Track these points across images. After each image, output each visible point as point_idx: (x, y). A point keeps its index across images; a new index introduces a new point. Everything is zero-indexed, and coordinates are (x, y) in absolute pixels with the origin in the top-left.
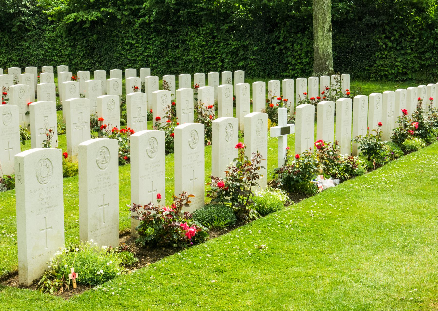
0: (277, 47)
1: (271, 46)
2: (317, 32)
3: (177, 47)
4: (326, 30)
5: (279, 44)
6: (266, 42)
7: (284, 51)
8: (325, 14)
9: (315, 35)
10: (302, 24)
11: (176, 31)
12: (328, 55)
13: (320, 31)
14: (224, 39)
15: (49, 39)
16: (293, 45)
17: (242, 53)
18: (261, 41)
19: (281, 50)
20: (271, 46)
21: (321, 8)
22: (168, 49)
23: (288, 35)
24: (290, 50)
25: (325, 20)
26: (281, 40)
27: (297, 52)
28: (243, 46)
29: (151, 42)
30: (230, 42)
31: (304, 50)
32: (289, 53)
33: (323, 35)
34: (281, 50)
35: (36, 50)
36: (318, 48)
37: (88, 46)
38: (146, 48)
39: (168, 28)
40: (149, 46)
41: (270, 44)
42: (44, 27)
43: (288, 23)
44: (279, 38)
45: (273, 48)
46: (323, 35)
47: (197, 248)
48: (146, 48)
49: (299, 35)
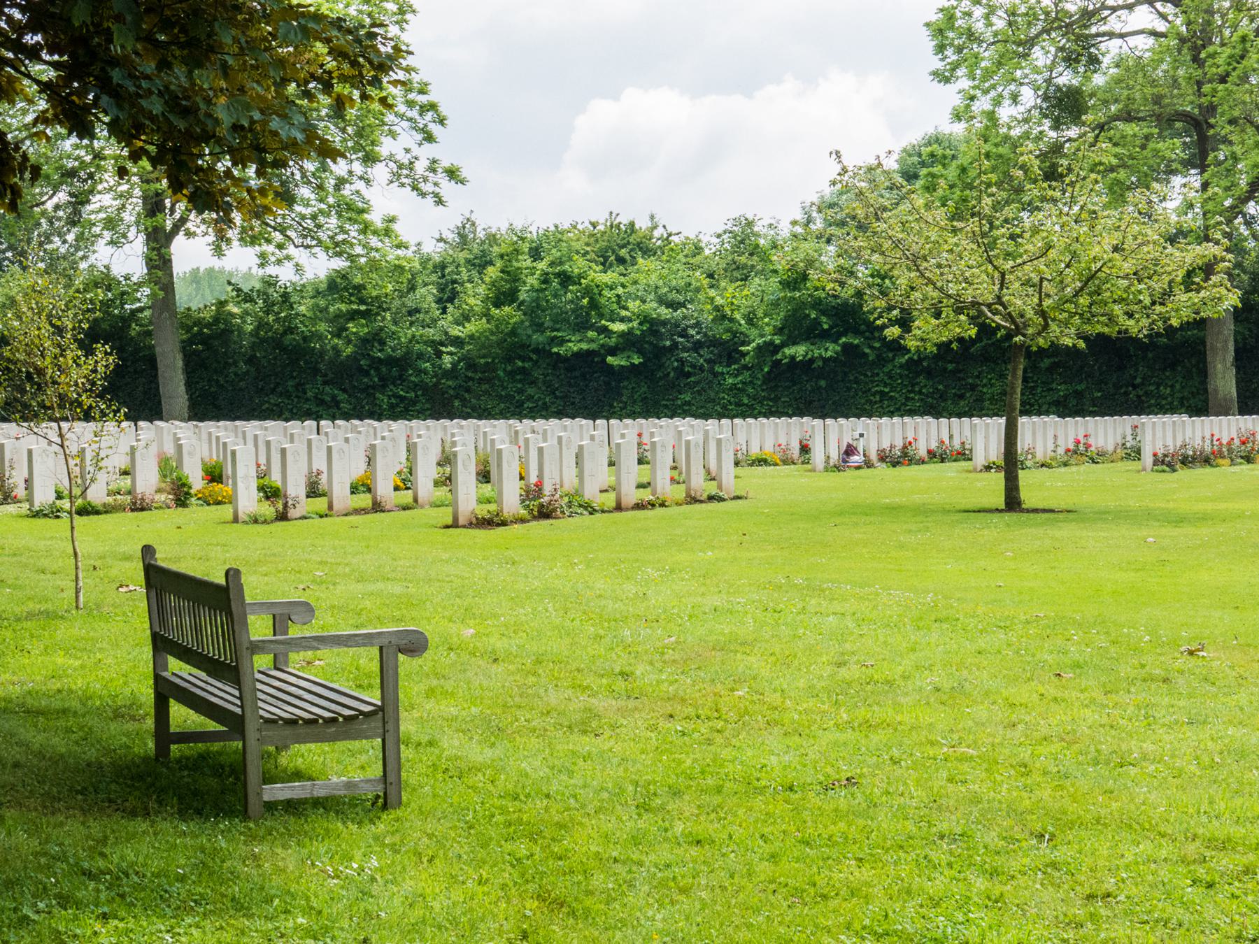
0: (1134, 392)
1: (1122, 391)
2: (1215, 367)
3: (961, 397)
4: (1229, 364)
5: (1135, 387)
6: (1114, 385)
7: (1143, 398)
8: (1226, 342)
9: (1210, 371)
10: (1171, 356)
11: (960, 371)
12: (1231, 400)
13: (1219, 366)
14: (1042, 383)
15: (731, 389)
16: (1158, 388)
17: (1074, 402)
18: (1106, 384)
19: (1139, 397)
20: (1122, 391)
21: (1220, 333)
22: (945, 400)
23: (1149, 373)
24: (1153, 396)
25: (1225, 349)
26: (1138, 381)
27: (1166, 399)
28: (1076, 392)
29: (917, 389)
30: (1054, 386)
31: (1178, 395)
32: (1153, 401)
33: (1224, 372)
34: (1139, 397)
35: (702, 407)
36: (1216, 391)
37: (801, 398)
38: (907, 399)
39: (950, 367)
40: (912, 395)
41: (1121, 387)
42: (718, 369)
43: (1150, 355)
44: (1135, 378)
45: (1127, 394)
46: (1224, 372)
47: (96, 517)
48: (907, 399)
49: (1167, 374)
